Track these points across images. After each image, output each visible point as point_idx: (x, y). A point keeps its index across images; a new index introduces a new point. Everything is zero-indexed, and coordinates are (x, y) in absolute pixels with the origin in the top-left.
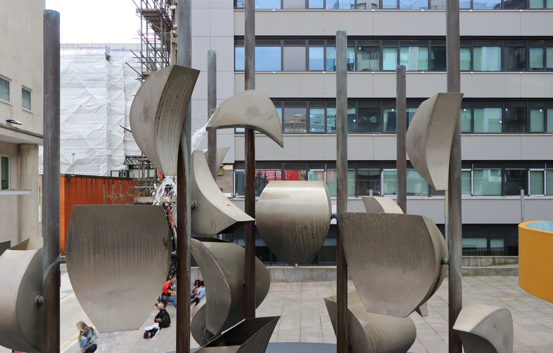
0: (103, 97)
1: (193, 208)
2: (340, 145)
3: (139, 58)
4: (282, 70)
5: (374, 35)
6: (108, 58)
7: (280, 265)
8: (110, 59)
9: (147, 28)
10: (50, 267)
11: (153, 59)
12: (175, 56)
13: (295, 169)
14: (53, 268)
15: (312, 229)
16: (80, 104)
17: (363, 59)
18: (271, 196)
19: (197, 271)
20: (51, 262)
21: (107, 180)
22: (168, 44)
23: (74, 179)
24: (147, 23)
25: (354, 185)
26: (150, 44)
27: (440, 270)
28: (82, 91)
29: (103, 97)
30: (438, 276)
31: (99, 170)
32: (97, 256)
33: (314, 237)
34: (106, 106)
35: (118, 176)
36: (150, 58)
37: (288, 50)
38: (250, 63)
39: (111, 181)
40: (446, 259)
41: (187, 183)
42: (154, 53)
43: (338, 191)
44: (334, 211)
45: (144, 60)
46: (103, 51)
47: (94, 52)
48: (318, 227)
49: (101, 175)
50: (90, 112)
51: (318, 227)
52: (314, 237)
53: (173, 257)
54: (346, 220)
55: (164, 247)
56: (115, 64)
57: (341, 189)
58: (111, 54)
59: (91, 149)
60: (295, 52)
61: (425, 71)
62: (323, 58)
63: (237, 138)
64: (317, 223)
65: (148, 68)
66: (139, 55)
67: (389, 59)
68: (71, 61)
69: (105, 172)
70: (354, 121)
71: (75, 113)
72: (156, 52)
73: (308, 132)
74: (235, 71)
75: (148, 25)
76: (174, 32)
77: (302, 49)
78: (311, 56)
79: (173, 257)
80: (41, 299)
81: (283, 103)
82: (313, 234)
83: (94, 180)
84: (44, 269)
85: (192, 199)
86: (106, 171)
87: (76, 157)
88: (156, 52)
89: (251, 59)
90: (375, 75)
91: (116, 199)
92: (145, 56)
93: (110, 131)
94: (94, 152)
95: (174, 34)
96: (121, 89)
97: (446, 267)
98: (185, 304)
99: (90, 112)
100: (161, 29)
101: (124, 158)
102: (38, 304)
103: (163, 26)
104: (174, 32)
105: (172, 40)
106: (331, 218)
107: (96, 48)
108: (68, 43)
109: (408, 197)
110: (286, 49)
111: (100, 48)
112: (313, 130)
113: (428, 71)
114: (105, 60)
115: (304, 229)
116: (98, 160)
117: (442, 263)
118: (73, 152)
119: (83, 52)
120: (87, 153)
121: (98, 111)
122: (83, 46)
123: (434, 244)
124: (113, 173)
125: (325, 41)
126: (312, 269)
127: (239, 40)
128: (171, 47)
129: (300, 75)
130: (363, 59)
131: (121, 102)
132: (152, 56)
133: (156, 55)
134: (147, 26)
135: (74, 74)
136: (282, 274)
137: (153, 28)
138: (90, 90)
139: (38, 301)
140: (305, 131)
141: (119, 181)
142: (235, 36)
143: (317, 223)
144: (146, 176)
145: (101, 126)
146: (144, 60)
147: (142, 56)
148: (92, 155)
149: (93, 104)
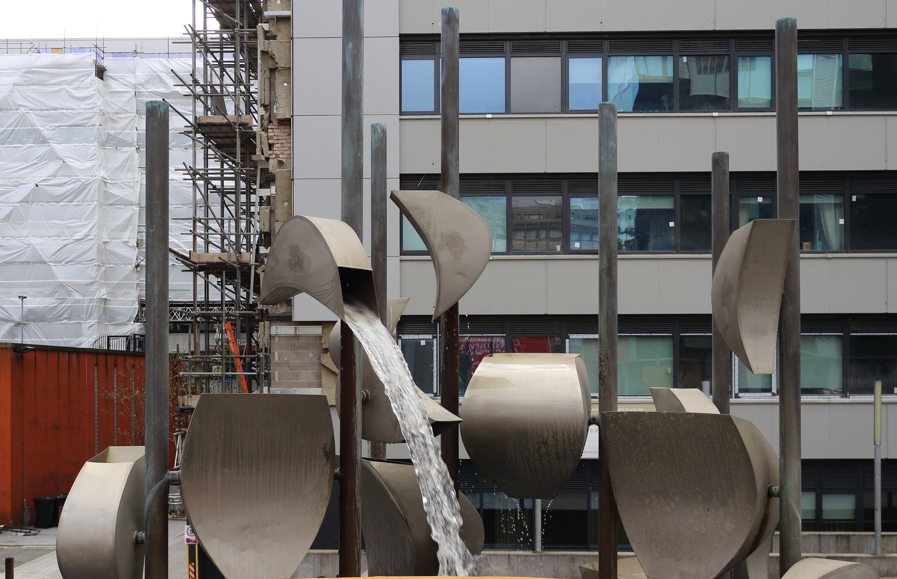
0: (89, 164)
1: (365, 402)
2: (605, 298)
3: (188, 86)
4: (508, 110)
5: (718, 29)
6: (101, 72)
7: (501, 548)
8: (106, 73)
9: (205, 18)
10: (156, 487)
11: (218, 89)
12: (267, 82)
13: (536, 333)
14: (160, 488)
15: (556, 446)
16: (37, 181)
17: (699, 72)
18: (492, 382)
19: (317, 559)
20: (157, 478)
21: (102, 358)
22: (252, 50)
23: (32, 355)
24: (205, 6)
25: (670, 370)
26: (212, 53)
27: (767, 506)
28: (42, 150)
29: (89, 164)
30: (762, 515)
31: (79, 334)
32: (226, 470)
33: (559, 458)
34: (96, 186)
35: (123, 348)
36: (212, 86)
37: (524, 65)
38: (450, 157)
39: (111, 360)
40: (776, 489)
41: (357, 362)
42: (218, 70)
43: (601, 377)
44: (595, 411)
45: (199, 90)
46: (89, 58)
47: (69, 58)
48: (567, 442)
49: (86, 345)
50: (57, 199)
51: (567, 442)
52: (559, 458)
53: (336, 477)
54: (612, 425)
55: (324, 460)
56: (115, 86)
57: (605, 374)
58: (107, 63)
59: (62, 285)
60: (536, 70)
61: (836, 109)
62: (599, 81)
63: (405, 264)
64: (563, 434)
65: (207, 109)
66: (189, 81)
67: (755, 80)
68: (15, 79)
69: (92, 340)
70: (672, 224)
71: (25, 201)
72: (223, 70)
73: (567, 250)
74: (401, 113)
75: (208, 10)
76: (266, 26)
77: (553, 63)
78: (573, 79)
79: (336, 477)
80: (142, 535)
81: (509, 184)
82: (557, 453)
83: (74, 357)
84: (146, 489)
85: (364, 387)
86: (95, 337)
87: (30, 304)
88: (223, 70)
89: (452, 150)
90: (718, 120)
91: (126, 400)
92: (202, 82)
93: (105, 243)
94: (69, 293)
95: (266, 32)
96: (130, 145)
97: (776, 501)
98: (354, 551)
99: (57, 199)
100: (237, 21)
101: (137, 306)
102: (138, 543)
103: (242, 12)
104: (266, 26)
105: (261, 44)
106: (590, 424)
107: (72, 50)
108: (9, 38)
109: (804, 398)
110: (516, 62)
111: (82, 49)
112: (577, 245)
113: (842, 109)
114: (93, 77)
115: (542, 445)
116: (74, 314)
117: (770, 494)
118: (21, 291)
119: (47, 58)
120: (51, 295)
121: (76, 197)
122: (42, 45)
123: (752, 461)
124: (112, 341)
125: (606, 44)
126: (573, 558)
127: (409, 45)
128: (259, 61)
129: (548, 121)
130: (699, 72)
131: (130, 175)
132: (216, 81)
133: (222, 76)
134: (205, 13)
135: (22, 110)
136: (506, 566)
137: (218, 16)
138: (59, 148)
139: (137, 538)
140: (558, 248)
141: (130, 361)
142: (401, 36)
143: (563, 434)
144: (202, 348)
145: (84, 231)
146: (199, 90)
147: (196, 82)
148: (63, 300)
149: (66, 180)
